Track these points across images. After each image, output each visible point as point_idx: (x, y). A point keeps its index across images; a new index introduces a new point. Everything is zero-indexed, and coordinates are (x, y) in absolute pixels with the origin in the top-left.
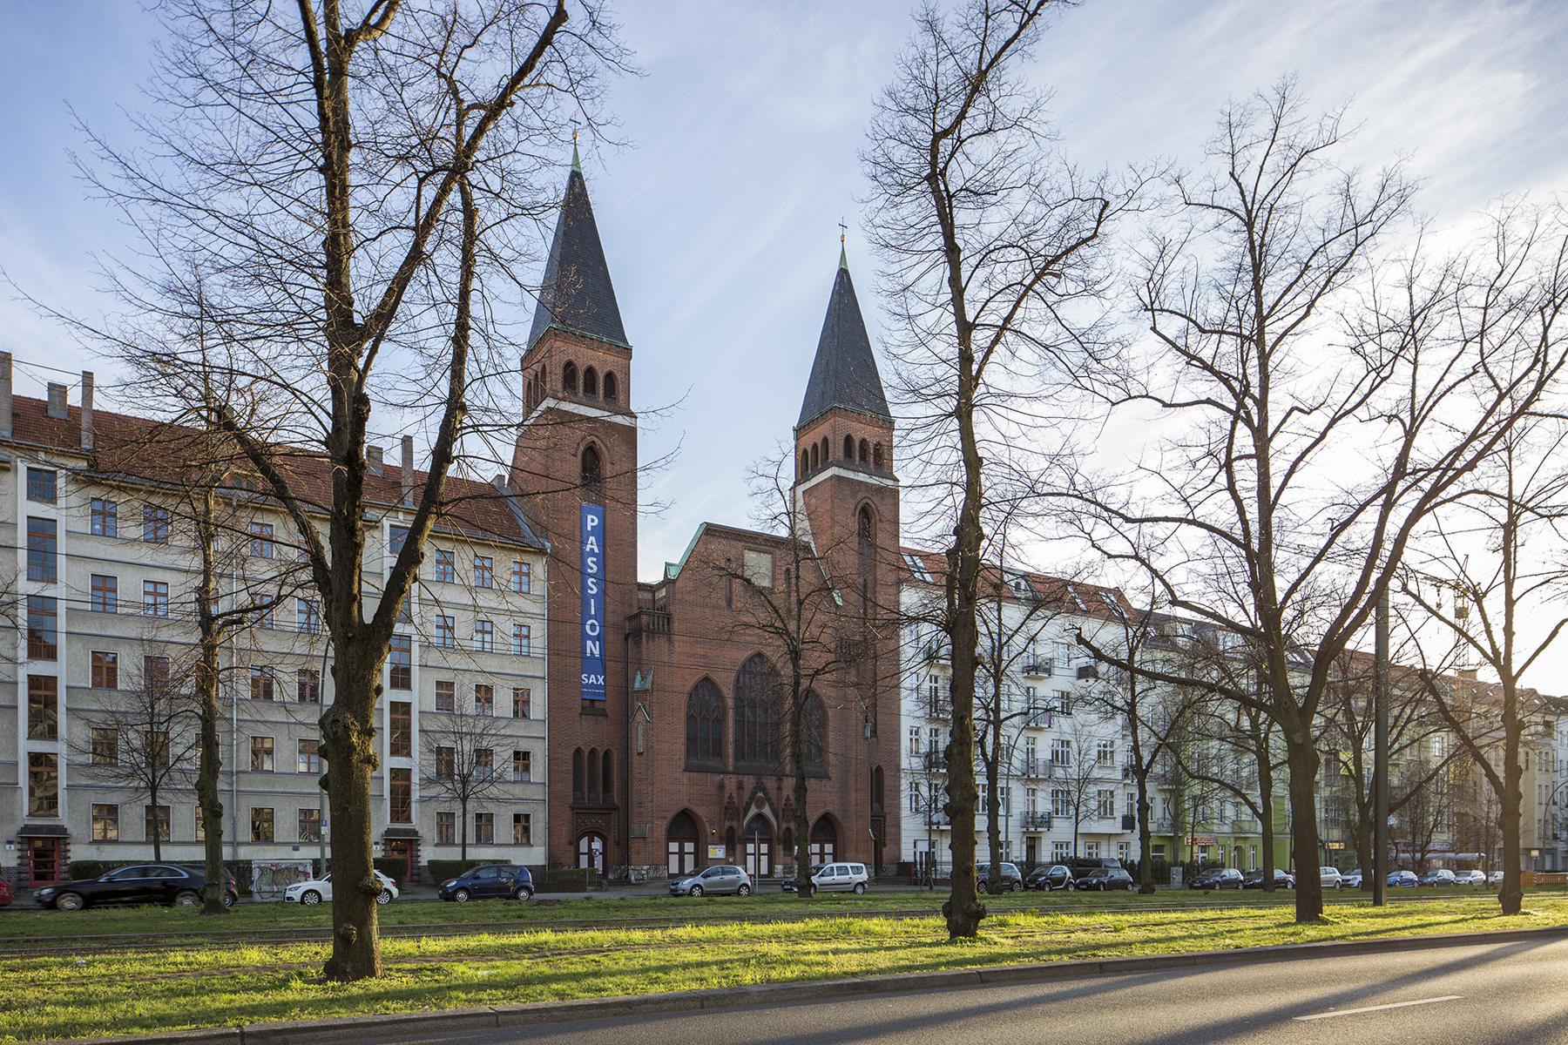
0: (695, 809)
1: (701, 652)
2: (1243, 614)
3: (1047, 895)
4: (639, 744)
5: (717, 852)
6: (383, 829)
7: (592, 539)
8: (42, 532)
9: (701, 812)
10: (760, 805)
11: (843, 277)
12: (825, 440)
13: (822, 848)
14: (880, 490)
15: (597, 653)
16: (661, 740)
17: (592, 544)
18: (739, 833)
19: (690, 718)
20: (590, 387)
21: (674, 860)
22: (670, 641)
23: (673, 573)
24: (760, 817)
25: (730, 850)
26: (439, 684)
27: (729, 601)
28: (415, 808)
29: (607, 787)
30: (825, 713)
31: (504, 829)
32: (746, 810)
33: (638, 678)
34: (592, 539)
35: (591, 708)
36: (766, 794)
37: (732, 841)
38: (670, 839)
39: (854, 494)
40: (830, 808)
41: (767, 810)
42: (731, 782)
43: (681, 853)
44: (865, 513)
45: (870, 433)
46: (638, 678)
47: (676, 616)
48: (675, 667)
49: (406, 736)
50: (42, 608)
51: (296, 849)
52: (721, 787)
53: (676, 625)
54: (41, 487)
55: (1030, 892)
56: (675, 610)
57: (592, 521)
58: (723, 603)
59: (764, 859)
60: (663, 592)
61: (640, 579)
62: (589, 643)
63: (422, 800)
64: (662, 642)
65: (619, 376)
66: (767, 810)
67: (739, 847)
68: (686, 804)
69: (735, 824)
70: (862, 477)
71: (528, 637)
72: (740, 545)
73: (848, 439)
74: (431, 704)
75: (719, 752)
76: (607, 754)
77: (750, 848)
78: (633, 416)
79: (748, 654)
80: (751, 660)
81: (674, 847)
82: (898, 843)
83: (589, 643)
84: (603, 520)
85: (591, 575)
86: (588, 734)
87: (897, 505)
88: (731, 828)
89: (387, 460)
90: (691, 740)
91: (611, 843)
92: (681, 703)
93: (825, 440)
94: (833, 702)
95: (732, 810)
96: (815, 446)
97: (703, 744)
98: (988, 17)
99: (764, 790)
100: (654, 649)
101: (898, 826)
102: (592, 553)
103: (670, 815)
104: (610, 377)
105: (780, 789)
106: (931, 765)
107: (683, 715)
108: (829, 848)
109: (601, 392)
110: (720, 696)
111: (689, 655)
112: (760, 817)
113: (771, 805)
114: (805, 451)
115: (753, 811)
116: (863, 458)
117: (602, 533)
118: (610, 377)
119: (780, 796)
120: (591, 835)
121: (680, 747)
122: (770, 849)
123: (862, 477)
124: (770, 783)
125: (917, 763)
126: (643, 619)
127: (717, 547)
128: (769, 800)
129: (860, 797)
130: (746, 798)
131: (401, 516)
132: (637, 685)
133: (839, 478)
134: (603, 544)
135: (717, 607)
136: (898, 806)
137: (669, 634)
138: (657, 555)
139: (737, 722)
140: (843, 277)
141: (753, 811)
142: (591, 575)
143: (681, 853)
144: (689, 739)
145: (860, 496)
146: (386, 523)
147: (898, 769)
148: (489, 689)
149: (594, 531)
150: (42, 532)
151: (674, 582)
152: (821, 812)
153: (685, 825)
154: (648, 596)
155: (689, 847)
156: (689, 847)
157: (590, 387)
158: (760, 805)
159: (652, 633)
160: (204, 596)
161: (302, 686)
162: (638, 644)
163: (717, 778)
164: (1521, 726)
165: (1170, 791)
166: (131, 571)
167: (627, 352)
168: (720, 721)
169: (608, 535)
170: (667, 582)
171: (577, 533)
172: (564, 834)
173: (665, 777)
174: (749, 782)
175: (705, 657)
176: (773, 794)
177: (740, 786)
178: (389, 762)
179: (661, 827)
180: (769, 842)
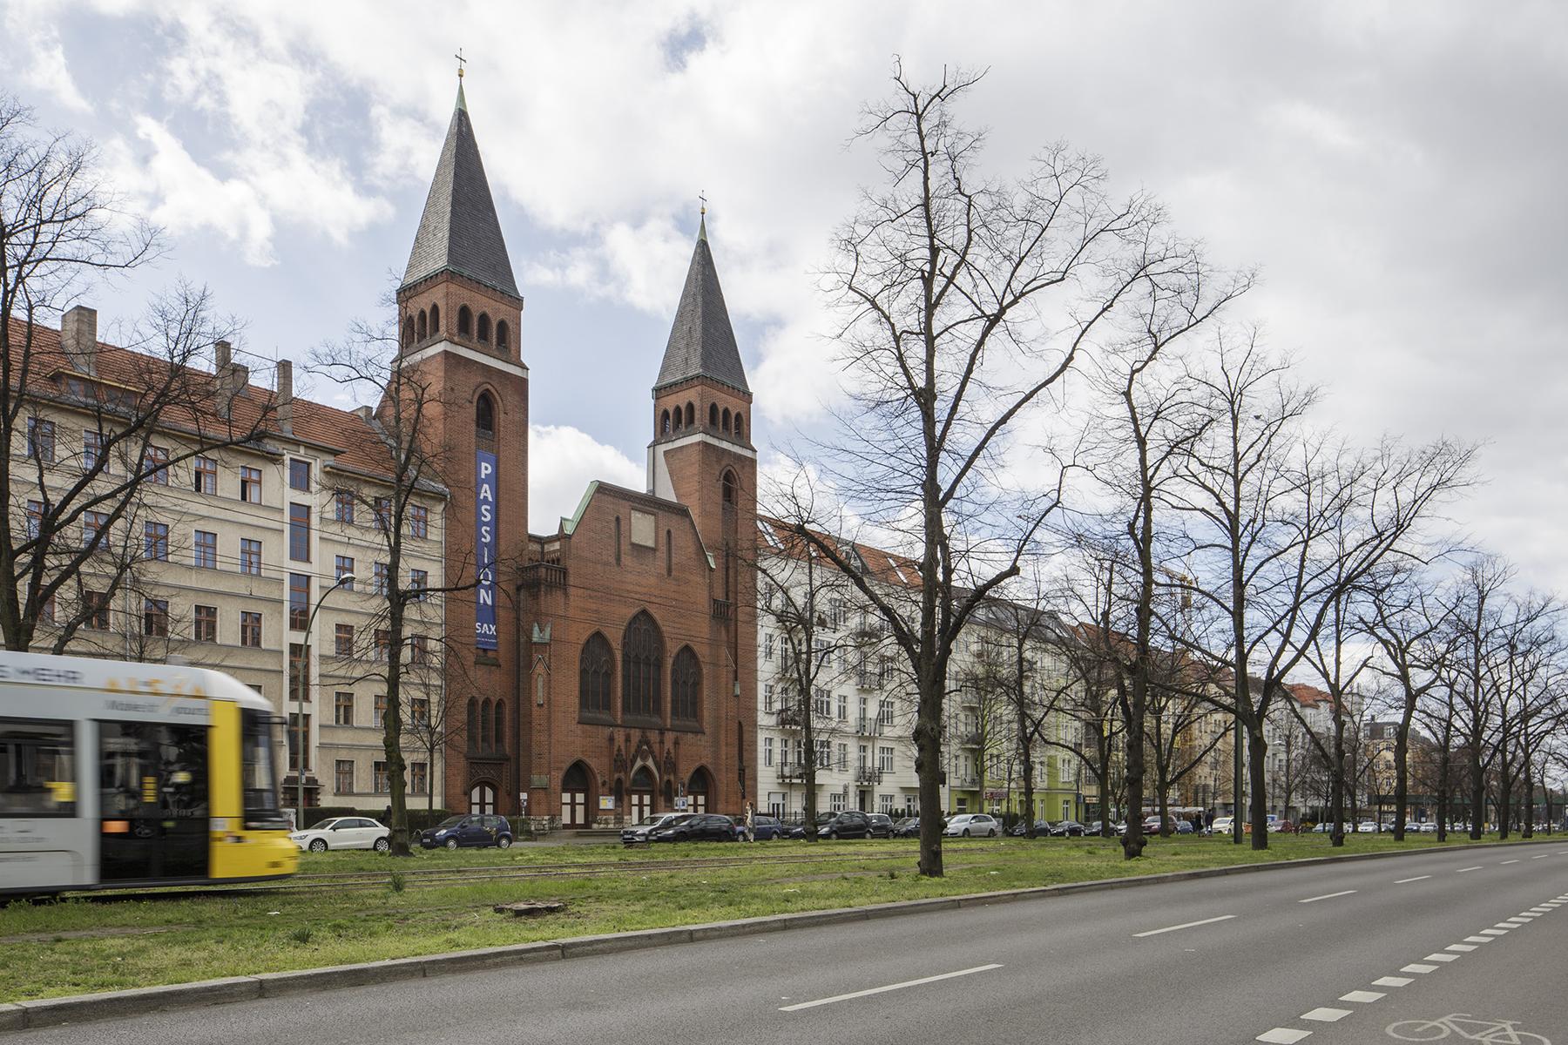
0: (588, 761)
1: (594, 607)
2: (1232, 655)
3: (1040, 839)
4: (539, 696)
5: (607, 803)
7: (486, 486)
9: (593, 763)
10: (644, 759)
12: (435, 309)
13: (573, 798)
14: (739, 458)
15: (489, 602)
16: (557, 690)
17: (486, 492)
18: (627, 784)
19: (583, 672)
20: (484, 335)
21: (566, 810)
22: (566, 595)
24: (644, 769)
25: (619, 801)
26: (339, 627)
27: (618, 559)
28: (314, 753)
29: (499, 739)
30: (699, 672)
32: (633, 762)
33: (536, 629)
34: (486, 486)
35: (485, 655)
37: (619, 793)
38: (565, 790)
39: (718, 462)
40: (704, 762)
41: (650, 763)
42: (620, 736)
43: (573, 804)
44: (728, 477)
45: (496, 311)
46: (536, 629)
49: (307, 683)
50: (301, 583)
52: (611, 739)
53: (571, 580)
54: (301, 480)
56: (572, 565)
57: (486, 469)
58: (612, 560)
59: (580, 810)
63: (322, 746)
64: (558, 596)
65: (511, 326)
66: (650, 763)
67: (626, 799)
68: (579, 756)
69: (622, 775)
71: (259, 554)
72: (627, 504)
73: (714, 408)
75: (608, 706)
76: (500, 704)
79: (635, 610)
80: (635, 617)
81: (566, 797)
85: (486, 524)
86: (488, 684)
87: (754, 474)
88: (619, 779)
91: (502, 793)
92: (574, 654)
94: (707, 660)
95: (620, 763)
96: (423, 313)
97: (593, 697)
98: (919, 117)
99: (648, 743)
100: (552, 602)
101: (755, 779)
103: (566, 766)
104: (738, 416)
105: (662, 742)
106: (783, 722)
108: (701, 800)
109: (494, 341)
110: (610, 650)
111: (584, 610)
112: (644, 769)
115: (639, 763)
117: (496, 480)
119: (661, 748)
120: (483, 784)
122: (652, 800)
123: (725, 445)
124: (653, 736)
125: (772, 720)
126: (539, 573)
127: (608, 502)
128: (652, 753)
129: (728, 752)
130: (633, 750)
132: (536, 637)
133: (706, 444)
135: (607, 564)
138: (551, 506)
139: (624, 677)
141: (639, 763)
143: (573, 804)
146: (287, 458)
148: (211, 612)
149: (487, 480)
150: (301, 514)
151: (569, 537)
153: (578, 777)
154: (535, 547)
155: (580, 798)
156: (580, 798)
157: (484, 335)
158: (644, 759)
159: (551, 586)
160: (390, 573)
161: (198, 623)
162: (536, 597)
164: (1344, 723)
165: (972, 750)
166: (228, 527)
167: (517, 302)
168: (609, 675)
169: (502, 485)
170: (561, 536)
171: (473, 479)
172: (459, 782)
173: (562, 729)
174: (636, 735)
177: (628, 739)
179: (558, 776)
180: (651, 793)
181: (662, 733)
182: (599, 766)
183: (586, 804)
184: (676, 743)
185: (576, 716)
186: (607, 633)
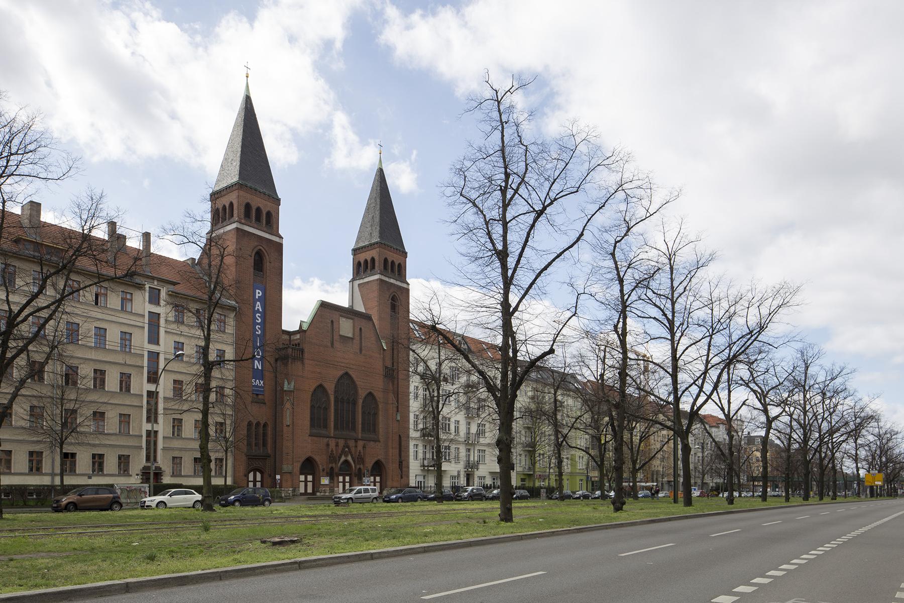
4: (288, 420)
5: (325, 481)
6: (141, 467)
8: (154, 318)
9: (317, 458)
10: (346, 456)
11: (248, 100)
12: (231, 204)
13: (306, 478)
16: (297, 417)
17: (258, 306)
18: (336, 470)
20: (258, 219)
21: (302, 485)
22: (303, 363)
23: (305, 327)
24: (346, 462)
29: (265, 445)
31: (111, 464)
32: (340, 458)
33: (286, 383)
35: (257, 397)
36: (349, 449)
37: (332, 475)
38: (301, 474)
42: (332, 443)
43: (306, 481)
44: (394, 299)
46: (286, 383)
47: (306, 350)
48: (302, 381)
51: (90, 478)
52: (328, 445)
53: (306, 355)
55: (552, 502)
57: (259, 293)
58: (329, 344)
59: (310, 485)
60: (298, 336)
61: (284, 328)
62: (256, 362)
63: (164, 449)
66: (349, 458)
67: (336, 478)
68: (309, 454)
69: (334, 465)
70: (392, 281)
74: (170, 394)
75: (326, 426)
77: (341, 479)
78: (281, 238)
79: (341, 373)
80: (342, 377)
81: (302, 478)
82: (408, 477)
83: (256, 362)
84: (264, 293)
85: (258, 324)
86: (260, 414)
89: (129, 243)
90: (312, 419)
91: (266, 475)
92: (307, 397)
93: (231, 204)
95: (333, 458)
96: (224, 207)
97: (318, 421)
99: (348, 447)
101: (408, 467)
102: (258, 311)
105: (356, 447)
106: (424, 435)
107: (309, 405)
112: (346, 462)
113: (352, 456)
114: (359, 263)
115: (343, 458)
116: (385, 267)
117: (263, 300)
118: (399, 265)
120: (255, 470)
121: (307, 422)
122: (350, 479)
123: (392, 281)
124: (351, 443)
125: (418, 434)
126: (290, 350)
128: (350, 453)
129: (393, 452)
131: (156, 283)
133: (381, 280)
134: (264, 307)
136: (408, 456)
137: (302, 360)
140: (248, 100)
141: (343, 458)
142: (258, 324)
143: (306, 481)
144: (311, 419)
145: (391, 291)
146: (147, 286)
147: (408, 436)
150: (154, 318)
151: (305, 331)
152: (376, 459)
153: (309, 466)
154: (287, 337)
155: (310, 478)
156: (310, 478)
158: (346, 456)
159: (295, 359)
160: (205, 351)
161: (95, 379)
162: (286, 365)
163: (326, 440)
165: (529, 451)
168: (326, 409)
170: (301, 331)
172: (242, 469)
173: (299, 440)
174: (341, 442)
175: (320, 373)
176: (353, 450)
177: (337, 445)
178: (147, 426)
179: (298, 466)
180: (350, 475)
181: (356, 440)
182: (321, 460)
183: (313, 481)
184: (364, 447)
185: (308, 432)
186: (326, 385)
